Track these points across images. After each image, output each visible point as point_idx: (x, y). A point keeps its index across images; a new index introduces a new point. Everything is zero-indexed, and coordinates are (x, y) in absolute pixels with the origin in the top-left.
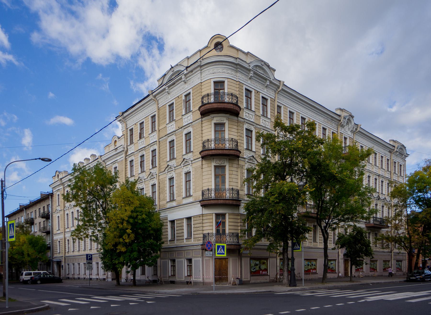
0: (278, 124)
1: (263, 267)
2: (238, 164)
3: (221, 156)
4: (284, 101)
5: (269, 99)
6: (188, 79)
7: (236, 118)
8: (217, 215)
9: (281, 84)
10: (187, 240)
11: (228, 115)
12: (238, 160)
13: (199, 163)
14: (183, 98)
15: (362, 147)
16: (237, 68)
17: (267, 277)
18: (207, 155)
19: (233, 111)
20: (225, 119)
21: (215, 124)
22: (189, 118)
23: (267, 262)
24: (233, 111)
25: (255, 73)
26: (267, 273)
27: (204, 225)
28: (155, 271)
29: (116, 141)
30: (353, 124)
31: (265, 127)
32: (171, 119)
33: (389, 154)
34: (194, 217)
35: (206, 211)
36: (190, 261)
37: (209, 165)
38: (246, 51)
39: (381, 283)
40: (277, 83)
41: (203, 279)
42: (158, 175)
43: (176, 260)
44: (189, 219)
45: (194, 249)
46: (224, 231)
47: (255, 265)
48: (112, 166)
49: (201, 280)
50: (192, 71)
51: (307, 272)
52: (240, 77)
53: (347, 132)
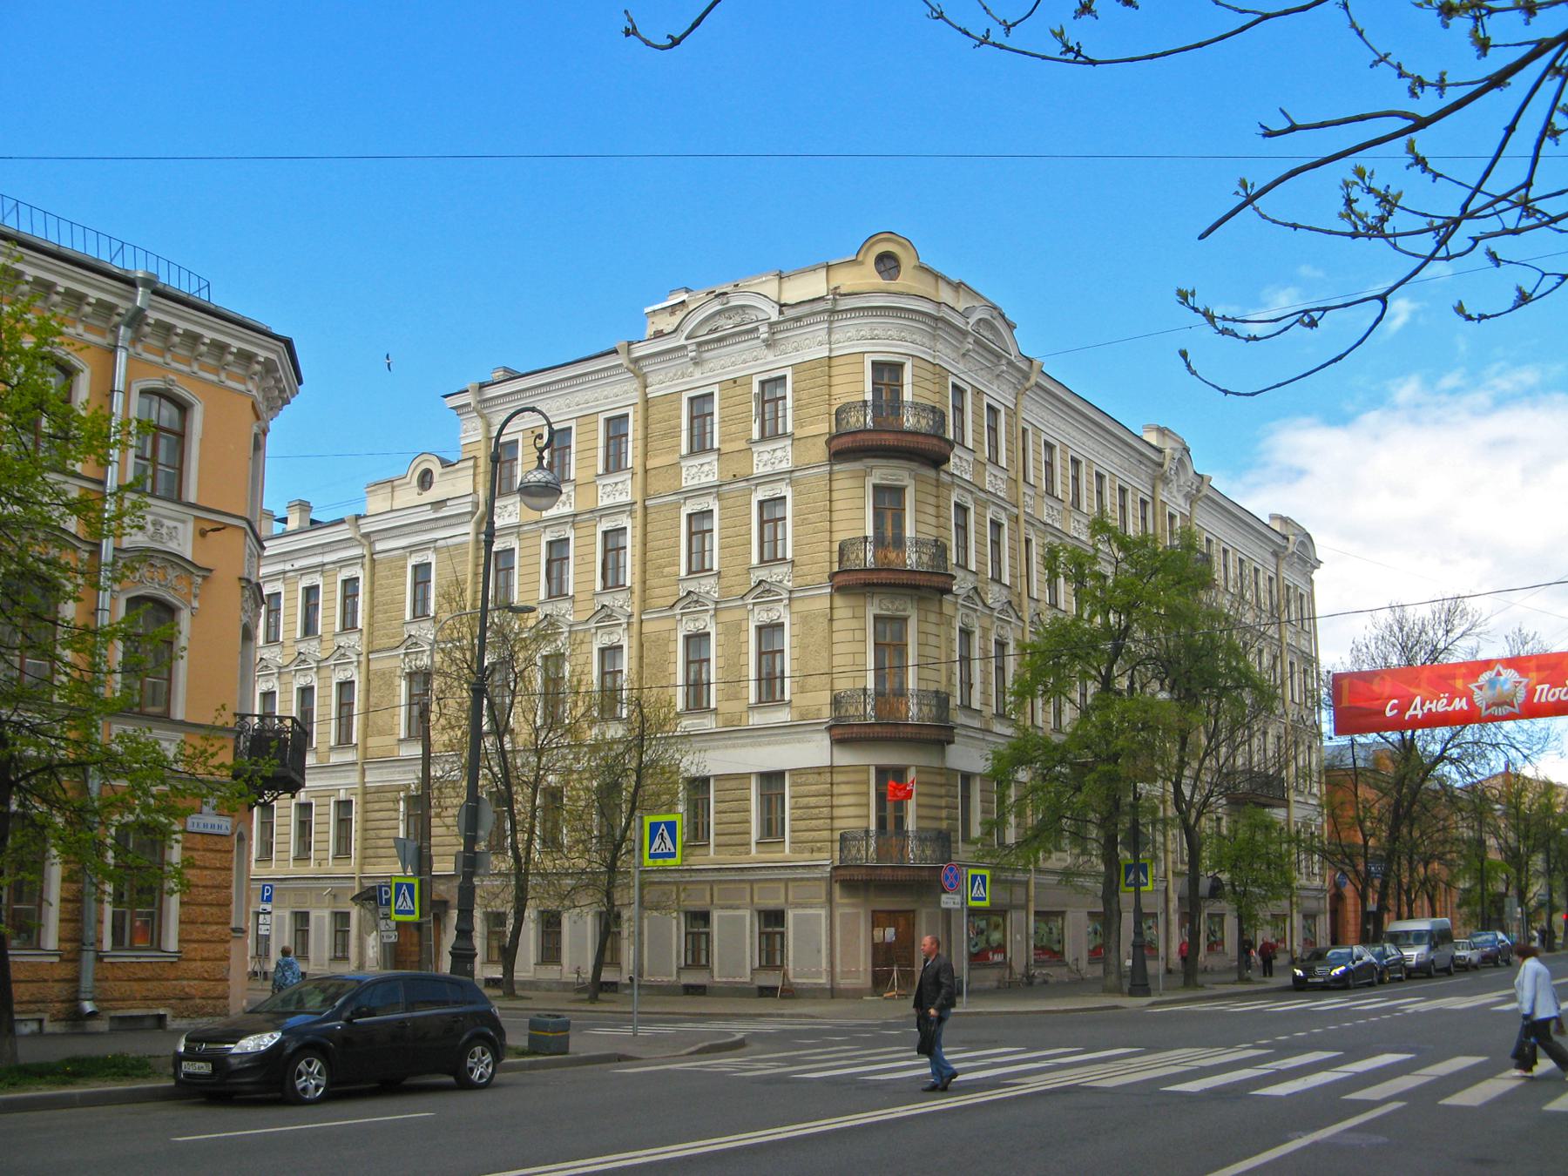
0: (1099, 526)
1: (996, 937)
2: (941, 613)
3: (891, 585)
4: (1033, 413)
5: (1003, 409)
6: (778, 336)
7: (931, 473)
8: (882, 772)
9: (1035, 367)
11: (914, 465)
12: (940, 601)
13: (819, 602)
14: (756, 388)
15: (1209, 541)
16: (935, 329)
18: (851, 583)
19: (929, 454)
20: (906, 474)
21: (877, 488)
22: (773, 458)
24: (929, 454)
25: (977, 342)
27: (836, 801)
28: (339, 947)
29: (427, 473)
30: (1191, 473)
31: (995, 495)
32: (699, 445)
33: (1273, 560)
34: (796, 772)
35: (845, 758)
37: (859, 612)
38: (956, 279)
39: (71, 1096)
40: (1024, 366)
42: (635, 619)
44: (772, 780)
45: (795, 880)
46: (900, 821)
48: (405, 559)
49: (824, 980)
50: (798, 319)
51: (978, 959)
52: (945, 355)
53: (1174, 501)
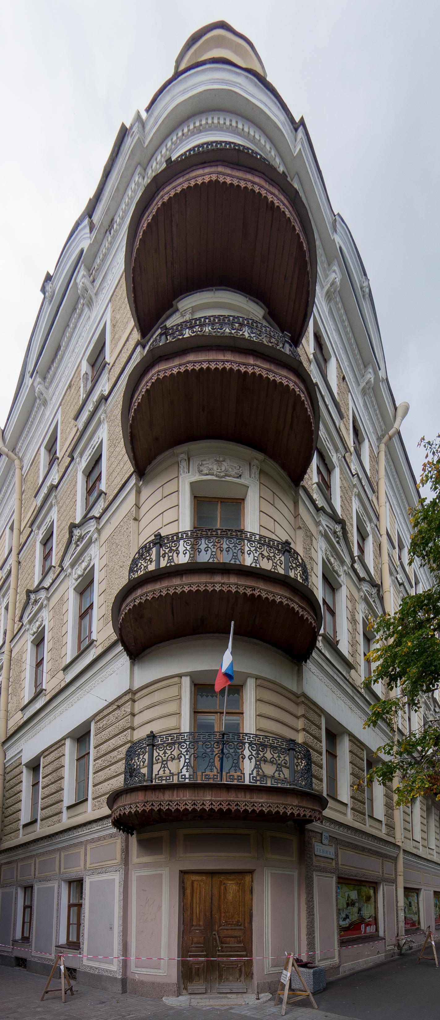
10: (73, 812)
17: (379, 945)
23: (375, 892)
26: (377, 930)
36: (77, 884)
41: (125, 965)
43: (36, 888)
45: (93, 841)
47: (348, 905)
